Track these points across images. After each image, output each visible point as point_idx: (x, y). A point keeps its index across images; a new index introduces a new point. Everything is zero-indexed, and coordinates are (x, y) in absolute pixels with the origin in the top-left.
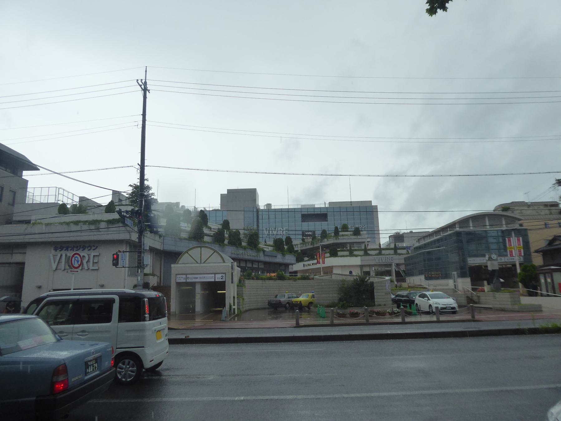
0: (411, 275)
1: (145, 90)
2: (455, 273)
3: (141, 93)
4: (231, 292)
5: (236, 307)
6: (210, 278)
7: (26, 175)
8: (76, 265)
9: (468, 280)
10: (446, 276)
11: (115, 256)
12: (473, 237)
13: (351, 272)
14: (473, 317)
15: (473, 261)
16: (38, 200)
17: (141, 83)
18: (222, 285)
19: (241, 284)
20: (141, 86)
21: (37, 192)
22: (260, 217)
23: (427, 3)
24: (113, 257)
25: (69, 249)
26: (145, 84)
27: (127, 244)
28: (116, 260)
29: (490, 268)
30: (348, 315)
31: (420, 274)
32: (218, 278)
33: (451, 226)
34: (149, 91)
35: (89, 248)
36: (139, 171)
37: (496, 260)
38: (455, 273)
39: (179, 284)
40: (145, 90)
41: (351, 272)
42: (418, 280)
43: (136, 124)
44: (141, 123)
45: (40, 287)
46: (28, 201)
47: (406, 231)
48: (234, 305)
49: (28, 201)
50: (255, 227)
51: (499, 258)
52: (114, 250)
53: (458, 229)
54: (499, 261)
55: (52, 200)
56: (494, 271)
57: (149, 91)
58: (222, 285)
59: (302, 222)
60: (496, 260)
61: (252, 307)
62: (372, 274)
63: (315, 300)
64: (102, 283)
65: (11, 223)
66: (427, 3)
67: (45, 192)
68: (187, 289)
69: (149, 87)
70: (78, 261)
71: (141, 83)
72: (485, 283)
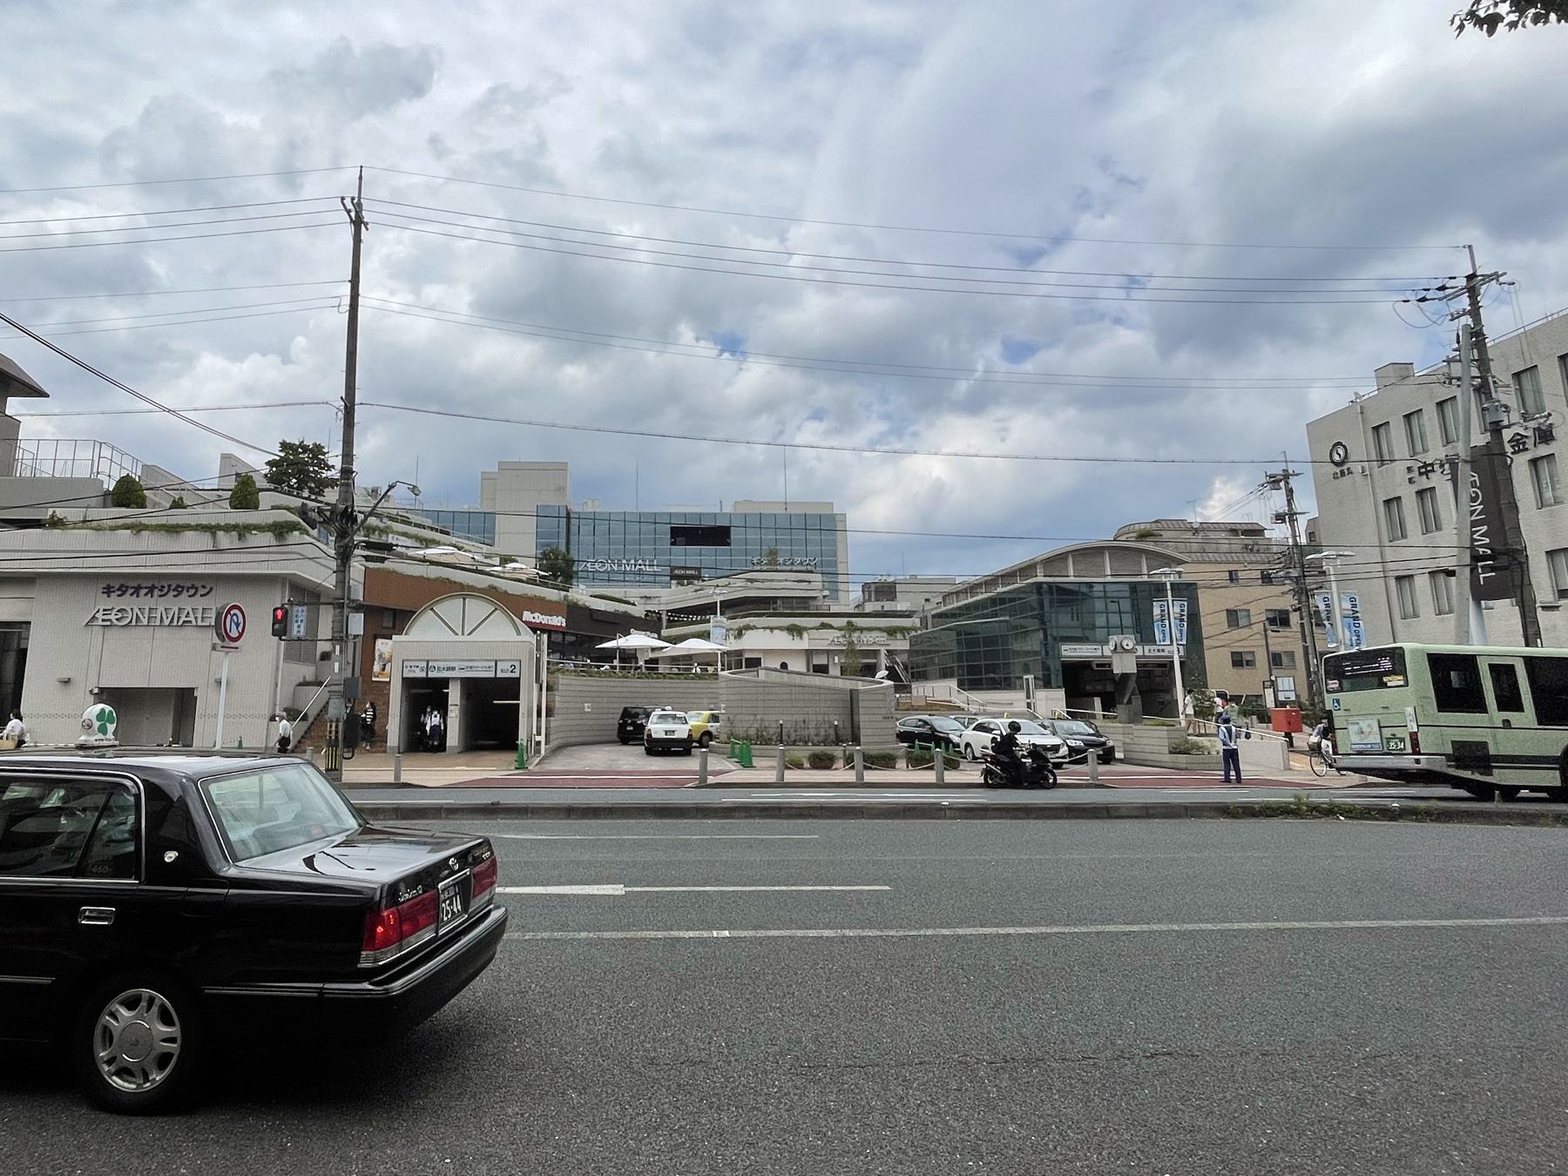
0: (922, 676)
1: (358, 222)
3: (350, 229)
4: (529, 699)
5: (542, 738)
8: (234, 634)
9: (1061, 693)
10: (1006, 684)
11: (279, 613)
12: (1067, 596)
13: (784, 666)
14: (397, 776)
15: (1072, 652)
16: (46, 470)
17: (350, 206)
18: (511, 687)
20: (349, 212)
21: (47, 452)
22: (574, 529)
24: (275, 616)
25: (156, 592)
26: (359, 207)
27: (284, 585)
28: (280, 622)
29: (1117, 670)
30: (807, 765)
31: (945, 674)
33: (1027, 570)
34: (366, 224)
35: (192, 592)
36: (341, 415)
40: (358, 222)
41: (784, 666)
42: (944, 689)
43: (335, 302)
44: (347, 301)
45: (67, 682)
46: (23, 470)
48: (539, 734)
49: (23, 470)
50: (563, 548)
51: (1140, 648)
52: (278, 598)
53: (1041, 579)
54: (1140, 653)
55: (82, 472)
56: (1125, 676)
57: (366, 224)
58: (511, 687)
59: (256, 508)
61: (573, 740)
62: (835, 671)
63: (713, 727)
64: (65, 676)
67: (65, 452)
68: (426, 694)
69: (366, 216)
70: (237, 625)
71: (350, 206)
72: (1097, 701)
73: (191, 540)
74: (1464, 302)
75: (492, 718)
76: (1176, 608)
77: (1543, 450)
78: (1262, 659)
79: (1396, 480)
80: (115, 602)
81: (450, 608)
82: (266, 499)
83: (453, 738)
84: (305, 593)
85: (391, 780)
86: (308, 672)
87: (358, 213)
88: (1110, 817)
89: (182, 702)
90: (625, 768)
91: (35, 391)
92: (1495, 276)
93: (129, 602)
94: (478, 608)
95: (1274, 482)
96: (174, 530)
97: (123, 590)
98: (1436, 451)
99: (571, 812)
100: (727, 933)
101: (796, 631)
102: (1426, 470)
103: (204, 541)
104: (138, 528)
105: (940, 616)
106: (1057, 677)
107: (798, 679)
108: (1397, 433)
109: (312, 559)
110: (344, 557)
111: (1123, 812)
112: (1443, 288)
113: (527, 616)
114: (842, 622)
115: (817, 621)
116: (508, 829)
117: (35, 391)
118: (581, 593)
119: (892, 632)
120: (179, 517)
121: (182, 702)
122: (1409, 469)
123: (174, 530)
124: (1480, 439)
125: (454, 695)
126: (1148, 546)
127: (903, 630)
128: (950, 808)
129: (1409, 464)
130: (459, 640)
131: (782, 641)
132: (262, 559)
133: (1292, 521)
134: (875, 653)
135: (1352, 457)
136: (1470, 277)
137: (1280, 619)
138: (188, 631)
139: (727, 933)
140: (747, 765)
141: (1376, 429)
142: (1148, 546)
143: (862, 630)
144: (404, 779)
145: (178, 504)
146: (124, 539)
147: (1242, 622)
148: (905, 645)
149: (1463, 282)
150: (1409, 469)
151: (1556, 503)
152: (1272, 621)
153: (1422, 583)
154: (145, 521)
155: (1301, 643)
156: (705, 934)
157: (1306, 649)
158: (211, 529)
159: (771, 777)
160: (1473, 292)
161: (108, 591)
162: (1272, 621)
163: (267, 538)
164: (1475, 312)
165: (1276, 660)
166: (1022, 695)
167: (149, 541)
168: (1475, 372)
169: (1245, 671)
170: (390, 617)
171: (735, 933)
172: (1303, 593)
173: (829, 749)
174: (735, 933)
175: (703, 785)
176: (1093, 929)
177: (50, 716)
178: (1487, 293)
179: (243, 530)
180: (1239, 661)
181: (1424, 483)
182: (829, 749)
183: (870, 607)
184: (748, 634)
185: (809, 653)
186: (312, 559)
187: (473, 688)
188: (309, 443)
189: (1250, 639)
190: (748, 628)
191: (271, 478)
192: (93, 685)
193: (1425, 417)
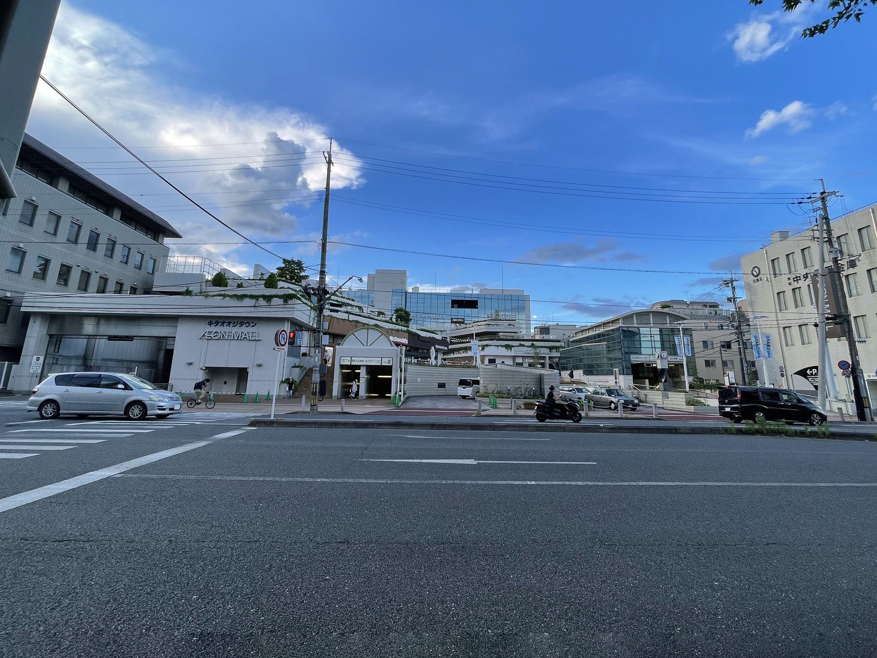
2: (617, 370)
3: (326, 166)
4: (395, 376)
5: (402, 393)
6: (375, 362)
7: (167, 241)
8: (283, 343)
9: (631, 377)
17: (327, 155)
19: (755, 422)
23: (285, 261)
32: (385, 362)
37: (666, 358)
38: (617, 370)
39: (342, 367)
45: (191, 364)
46: (168, 270)
47: (551, 323)
49: (168, 270)
53: (621, 325)
56: (663, 370)
58: (388, 370)
60: (666, 358)
64: (259, 363)
65: (148, 293)
66: (285, 261)
68: (351, 374)
72: (647, 381)
73: (248, 302)
74: (819, 204)
75: (379, 382)
76: (686, 339)
77: (851, 271)
78: (719, 363)
79: (783, 283)
80: (213, 329)
81: (362, 334)
82: (281, 284)
83: (363, 393)
84: (297, 326)
85: (340, 410)
86: (296, 361)
87: (330, 158)
88: (677, 433)
89: (242, 374)
90: (441, 407)
91: (175, 235)
92: (834, 193)
93: (219, 329)
94: (374, 334)
95: (726, 283)
96: (242, 297)
97: (217, 323)
98: (802, 271)
99: (433, 426)
100: (533, 483)
101: (508, 347)
102: (797, 279)
103: (252, 302)
104: (225, 296)
105: (574, 341)
106: (630, 371)
107: (509, 368)
108: (783, 262)
109: (303, 312)
110: (320, 309)
111: (683, 431)
112: (810, 198)
113: (391, 338)
114: (530, 343)
115: (518, 343)
116: (408, 433)
117: (175, 235)
118: (413, 328)
119: (551, 348)
120: (240, 292)
121: (242, 374)
122: (789, 279)
123: (242, 297)
124: (829, 263)
125: (363, 372)
126: (666, 310)
127: (556, 348)
128: (604, 427)
129: (789, 276)
130: (364, 350)
131: (503, 351)
132: (276, 309)
133: (734, 301)
134: (544, 358)
135: (762, 272)
136: (822, 193)
137: (727, 345)
138: (244, 342)
139: (533, 483)
140: (495, 407)
141: (773, 261)
142: (666, 310)
143: (538, 347)
144: (345, 410)
145: (240, 286)
146: (218, 301)
147: (710, 347)
148: (558, 355)
149: (819, 195)
150: (789, 279)
151: (858, 295)
152: (723, 346)
153: (795, 330)
154: (227, 293)
155: (738, 357)
156: (524, 483)
157: (741, 359)
158: (256, 297)
159: (511, 412)
160: (823, 199)
161: (210, 324)
162: (723, 346)
163: (281, 301)
164: (825, 208)
165: (724, 364)
166: (613, 377)
167: (228, 302)
168: (825, 235)
169: (711, 369)
170: (337, 338)
171: (538, 483)
172: (740, 333)
173: (532, 401)
174: (538, 483)
175: (479, 415)
176: (762, 484)
177: (185, 379)
178: (831, 201)
179: (268, 298)
180: (708, 363)
181: (795, 285)
182: (532, 401)
183: (537, 337)
184: (487, 349)
185: (514, 357)
186: (303, 312)
187: (373, 371)
188: (296, 260)
189: (714, 354)
190: (487, 346)
191: (280, 275)
192: (202, 366)
193: (796, 256)
